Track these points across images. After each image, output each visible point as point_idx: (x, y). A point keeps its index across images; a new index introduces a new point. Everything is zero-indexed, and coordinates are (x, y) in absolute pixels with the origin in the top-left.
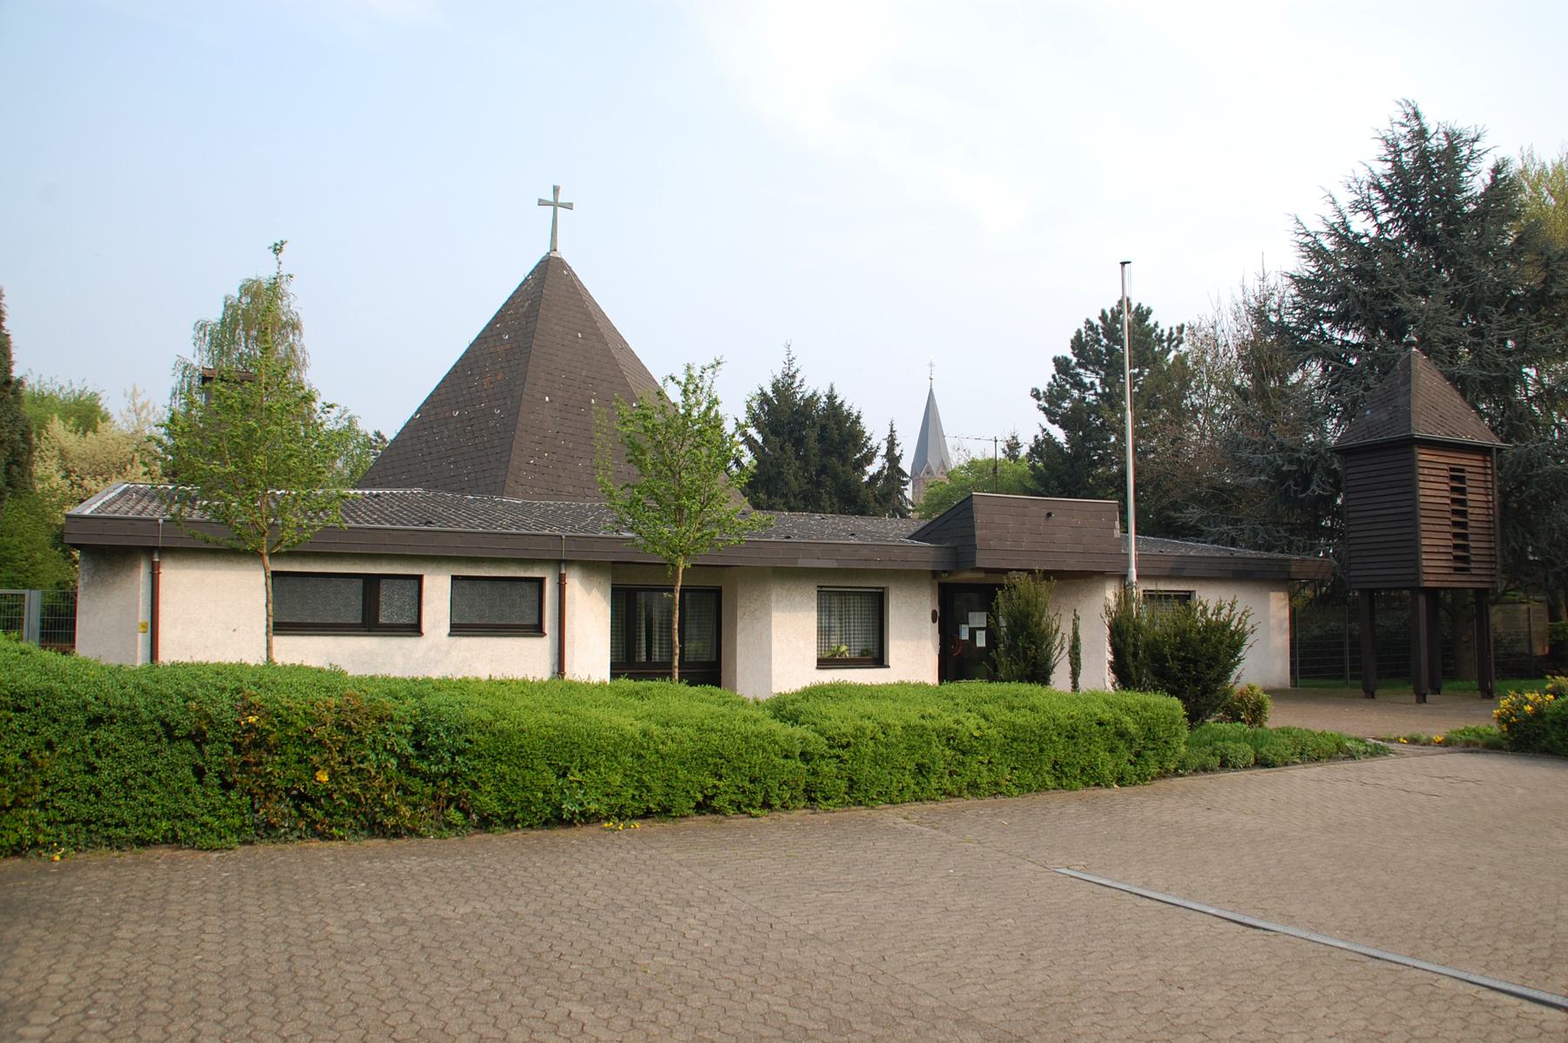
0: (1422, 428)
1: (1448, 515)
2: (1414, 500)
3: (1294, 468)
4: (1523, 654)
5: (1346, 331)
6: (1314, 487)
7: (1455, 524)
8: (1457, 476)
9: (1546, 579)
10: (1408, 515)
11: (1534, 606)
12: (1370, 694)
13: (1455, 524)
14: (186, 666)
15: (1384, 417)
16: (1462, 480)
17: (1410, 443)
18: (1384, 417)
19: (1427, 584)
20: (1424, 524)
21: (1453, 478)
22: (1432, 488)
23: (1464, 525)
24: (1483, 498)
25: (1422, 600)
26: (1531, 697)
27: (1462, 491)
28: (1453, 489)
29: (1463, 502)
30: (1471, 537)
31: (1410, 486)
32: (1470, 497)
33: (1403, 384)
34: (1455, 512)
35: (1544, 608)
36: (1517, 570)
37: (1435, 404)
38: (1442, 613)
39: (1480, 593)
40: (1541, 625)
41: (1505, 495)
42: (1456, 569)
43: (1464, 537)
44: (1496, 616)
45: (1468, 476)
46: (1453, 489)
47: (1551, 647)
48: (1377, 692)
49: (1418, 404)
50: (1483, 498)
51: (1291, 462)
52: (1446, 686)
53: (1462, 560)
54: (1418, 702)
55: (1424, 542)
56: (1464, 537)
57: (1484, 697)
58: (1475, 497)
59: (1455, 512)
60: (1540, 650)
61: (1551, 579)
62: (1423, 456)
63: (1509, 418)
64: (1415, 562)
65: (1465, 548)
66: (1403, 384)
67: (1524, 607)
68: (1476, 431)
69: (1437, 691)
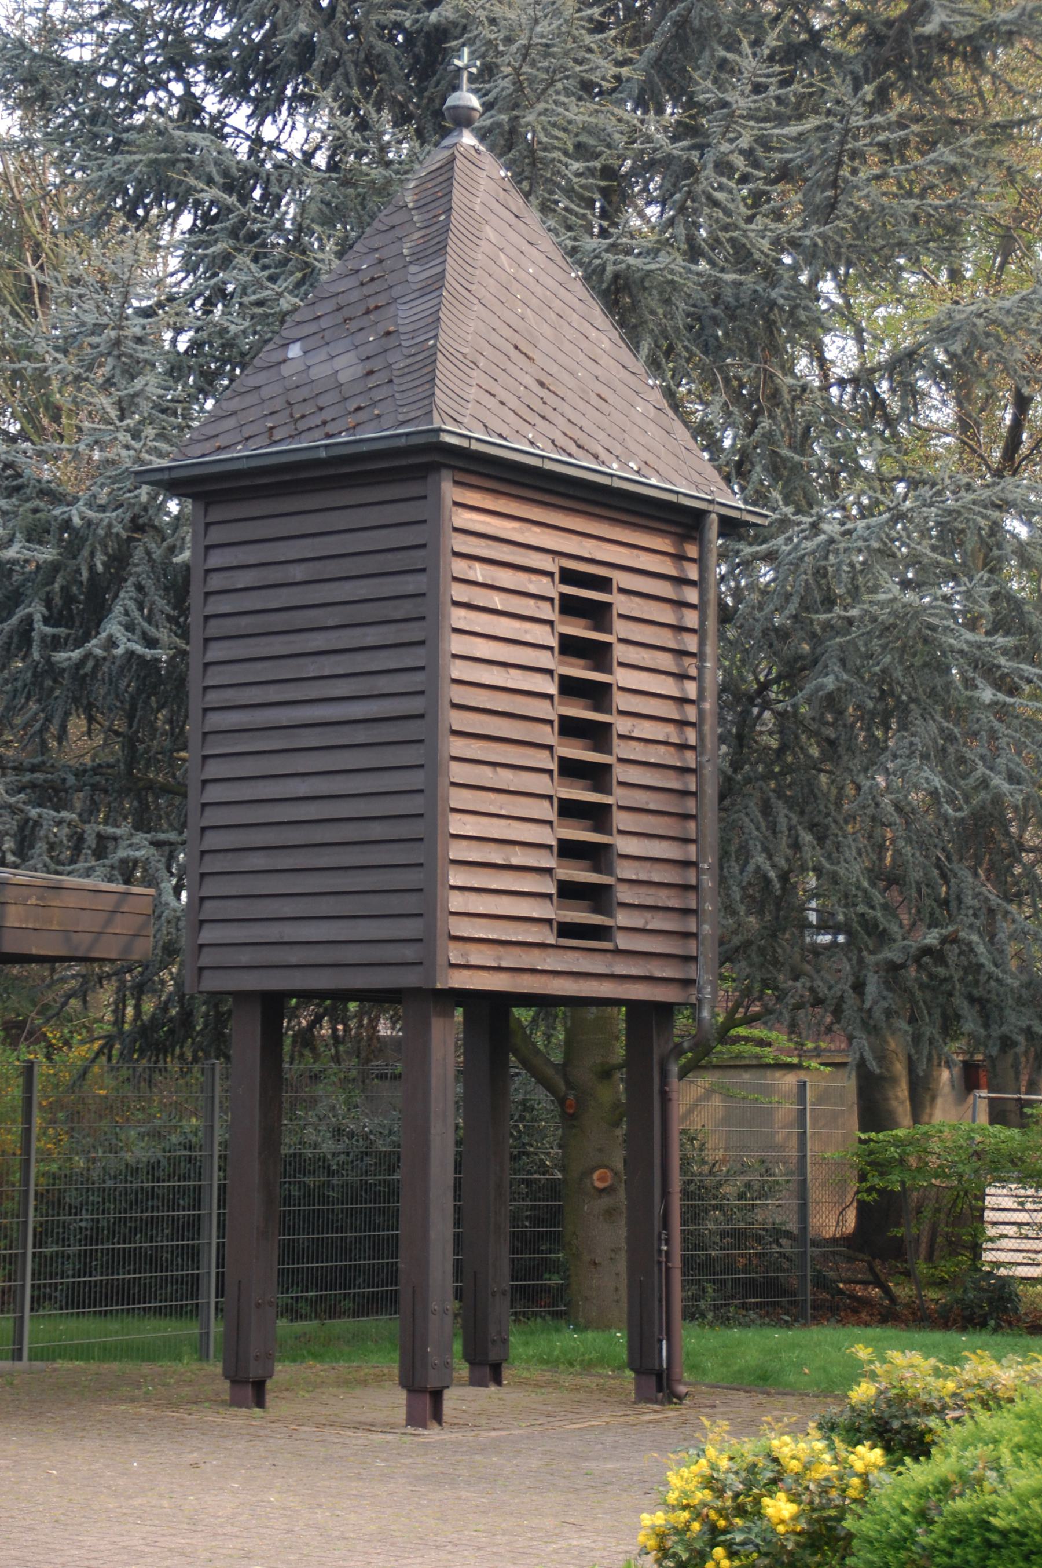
0: (472, 413)
1: (548, 735)
2: (429, 670)
3: (47, 554)
4: (778, 1233)
5: (263, 110)
6: (112, 627)
7: (570, 769)
8: (584, 599)
9: (859, 987)
10: (408, 727)
11: (819, 1078)
12: (251, 1388)
13: (570, 769)
14: (859, 1323)
15: (347, 366)
16: (598, 614)
17: (427, 461)
18: (347, 366)
19: (460, 980)
20: (462, 764)
21: (569, 607)
22: (493, 640)
23: (596, 776)
24: (667, 686)
25: (447, 1037)
26: (789, 1448)
27: (597, 654)
28: (569, 646)
29: (598, 694)
30: (621, 820)
31: (415, 621)
32: (622, 677)
33: (419, 257)
34: (569, 728)
35: (848, 1083)
36: (764, 947)
37: (522, 337)
38: (522, 1087)
39: (648, 1017)
40: (836, 1139)
41: (739, 700)
42: (566, 930)
43: (597, 816)
44: (697, 1106)
45: (621, 604)
46: (569, 646)
47: (863, 1209)
48: (283, 1371)
49: (465, 329)
50: (667, 686)
51: (36, 535)
52: (524, 1345)
53: (586, 901)
54: (415, 1420)
55: (458, 824)
56: (596, 776)
57: (643, 1397)
58: (639, 679)
59: (569, 728)
60: (834, 1219)
61: (872, 989)
62: (469, 514)
63: (769, 436)
64: (422, 899)
65: (596, 855)
66: (419, 257)
67: (789, 1080)
68: (651, 446)
69: (489, 1370)
